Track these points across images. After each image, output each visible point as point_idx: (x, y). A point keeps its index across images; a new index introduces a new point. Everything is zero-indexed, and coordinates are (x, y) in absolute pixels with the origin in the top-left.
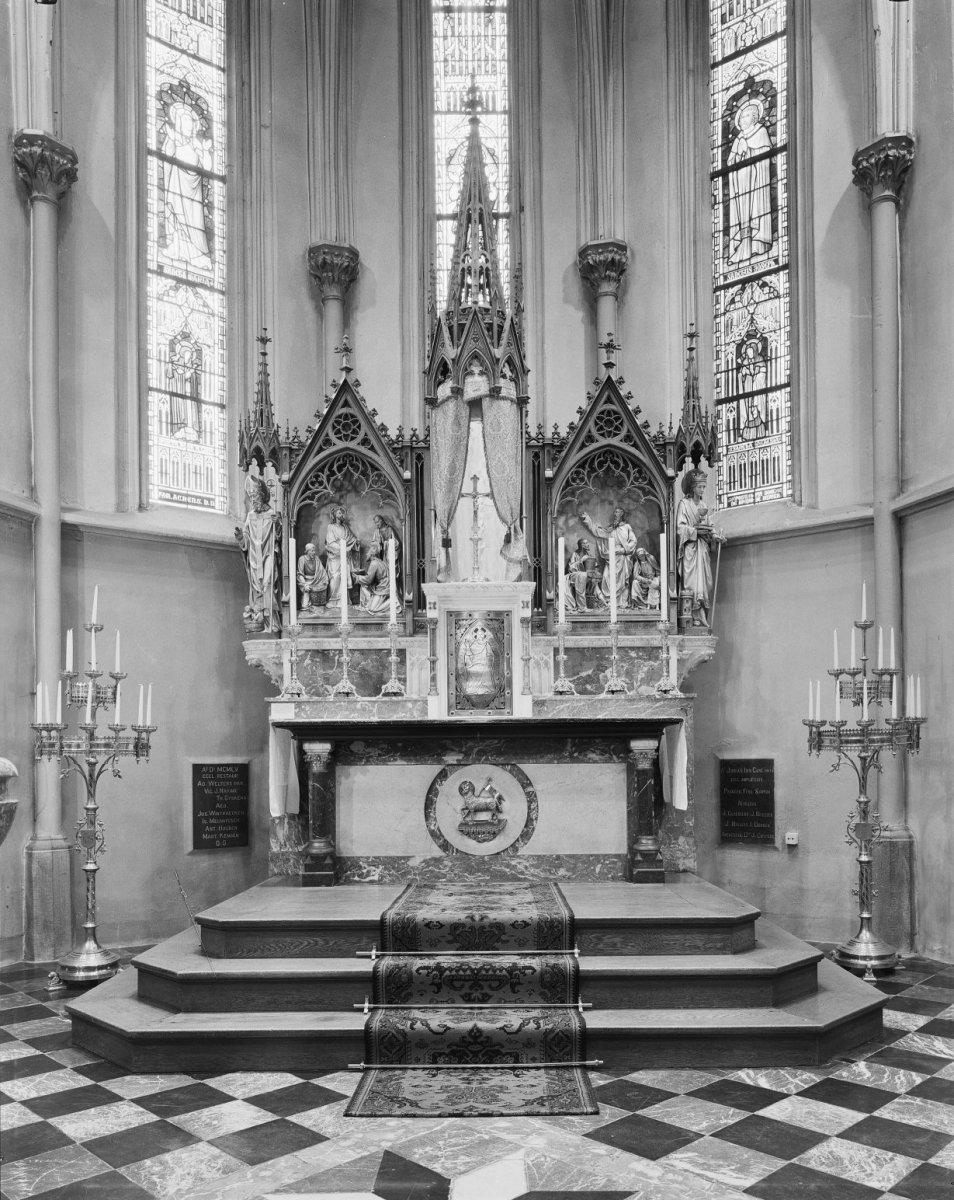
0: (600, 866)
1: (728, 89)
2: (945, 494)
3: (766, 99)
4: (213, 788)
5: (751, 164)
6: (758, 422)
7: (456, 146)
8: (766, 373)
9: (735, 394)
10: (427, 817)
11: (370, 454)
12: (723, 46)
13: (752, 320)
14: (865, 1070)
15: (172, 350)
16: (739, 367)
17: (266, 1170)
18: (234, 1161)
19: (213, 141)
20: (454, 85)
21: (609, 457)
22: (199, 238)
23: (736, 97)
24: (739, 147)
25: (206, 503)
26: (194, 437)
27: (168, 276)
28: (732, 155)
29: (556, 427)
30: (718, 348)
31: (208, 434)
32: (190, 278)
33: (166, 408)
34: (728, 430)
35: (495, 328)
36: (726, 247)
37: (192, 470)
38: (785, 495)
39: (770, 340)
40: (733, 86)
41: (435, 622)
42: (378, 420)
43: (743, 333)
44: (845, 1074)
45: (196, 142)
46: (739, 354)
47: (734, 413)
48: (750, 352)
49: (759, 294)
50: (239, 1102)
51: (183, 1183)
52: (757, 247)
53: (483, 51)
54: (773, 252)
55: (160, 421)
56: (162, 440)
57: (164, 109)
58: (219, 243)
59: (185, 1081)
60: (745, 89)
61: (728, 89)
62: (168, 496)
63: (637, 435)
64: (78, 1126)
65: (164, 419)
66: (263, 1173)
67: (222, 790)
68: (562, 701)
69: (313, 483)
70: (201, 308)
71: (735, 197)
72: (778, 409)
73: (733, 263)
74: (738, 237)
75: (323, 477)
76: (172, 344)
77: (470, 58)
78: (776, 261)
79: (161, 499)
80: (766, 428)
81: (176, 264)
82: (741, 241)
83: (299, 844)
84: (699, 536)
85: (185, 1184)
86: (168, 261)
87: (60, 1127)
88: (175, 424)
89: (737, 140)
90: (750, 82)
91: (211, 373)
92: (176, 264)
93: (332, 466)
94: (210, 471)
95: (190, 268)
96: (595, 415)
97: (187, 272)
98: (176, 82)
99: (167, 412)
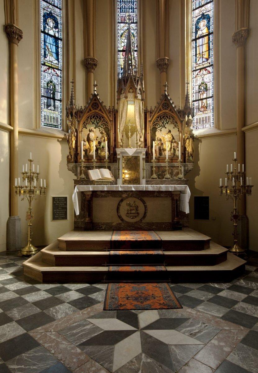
0: (164, 225)
1: (197, 17)
2: (256, 127)
3: (207, 20)
4: (58, 203)
5: (203, 38)
6: (204, 107)
7: (123, 32)
8: (207, 93)
9: (198, 99)
10: (118, 212)
11: (102, 113)
12: (196, 5)
13: (203, 79)
14: (243, 282)
15: (48, 85)
16: (199, 92)
17: (85, 311)
18: (75, 309)
19: (58, 29)
20: (123, 15)
21: (165, 115)
22: (54, 55)
23: (199, 19)
24: (200, 33)
25: (56, 127)
26: (53, 109)
27: (46, 66)
28: (198, 35)
29: (151, 107)
30: (194, 87)
31: (57, 108)
32: (52, 66)
33: (46, 101)
34: (196, 109)
35: (136, 80)
36: (196, 60)
37: (53, 118)
38: (211, 126)
39: (208, 85)
40: (198, 16)
41: (119, 159)
42: (104, 104)
43: (200, 83)
44: (238, 283)
45: (54, 29)
46: (199, 89)
47: (198, 104)
48: (202, 88)
49: (205, 72)
50: (74, 291)
51: (62, 315)
52: (204, 60)
53: (130, 6)
54: (209, 61)
55: (44, 105)
56: (45, 110)
57: (45, 21)
58: (60, 57)
59: (59, 285)
60: (202, 17)
61: (197, 17)
62: (46, 125)
63: (172, 110)
64: (31, 298)
65: (45, 104)
66: (85, 312)
67: (60, 204)
68: (153, 181)
69: (156, 121)
70: (55, 74)
71: (198, 46)
72: (210, 103)
73: (198, 64)
74: (199, 57)
75: (159, 120)
76: (48, 84)
77: (127, 8)
78: (210, 63)
79: (44, 125)
80: (207, 108)
81: (49, 62)
82: (200, 58)
83: (82, 219)
84: (191, 137)
85: (63, 315)
86: (47, 61)
87: (25, 298)
88: (48, 106)
89: (199, 31)
90: (203, 14)
91: (58, 92)
92: (49, 62)
93: (91, 116)
94: (57, 118)
95: (52, 64)
96: (162, 103)
97: (52, 65)
98: (48, 12)
99: (46, 102)
